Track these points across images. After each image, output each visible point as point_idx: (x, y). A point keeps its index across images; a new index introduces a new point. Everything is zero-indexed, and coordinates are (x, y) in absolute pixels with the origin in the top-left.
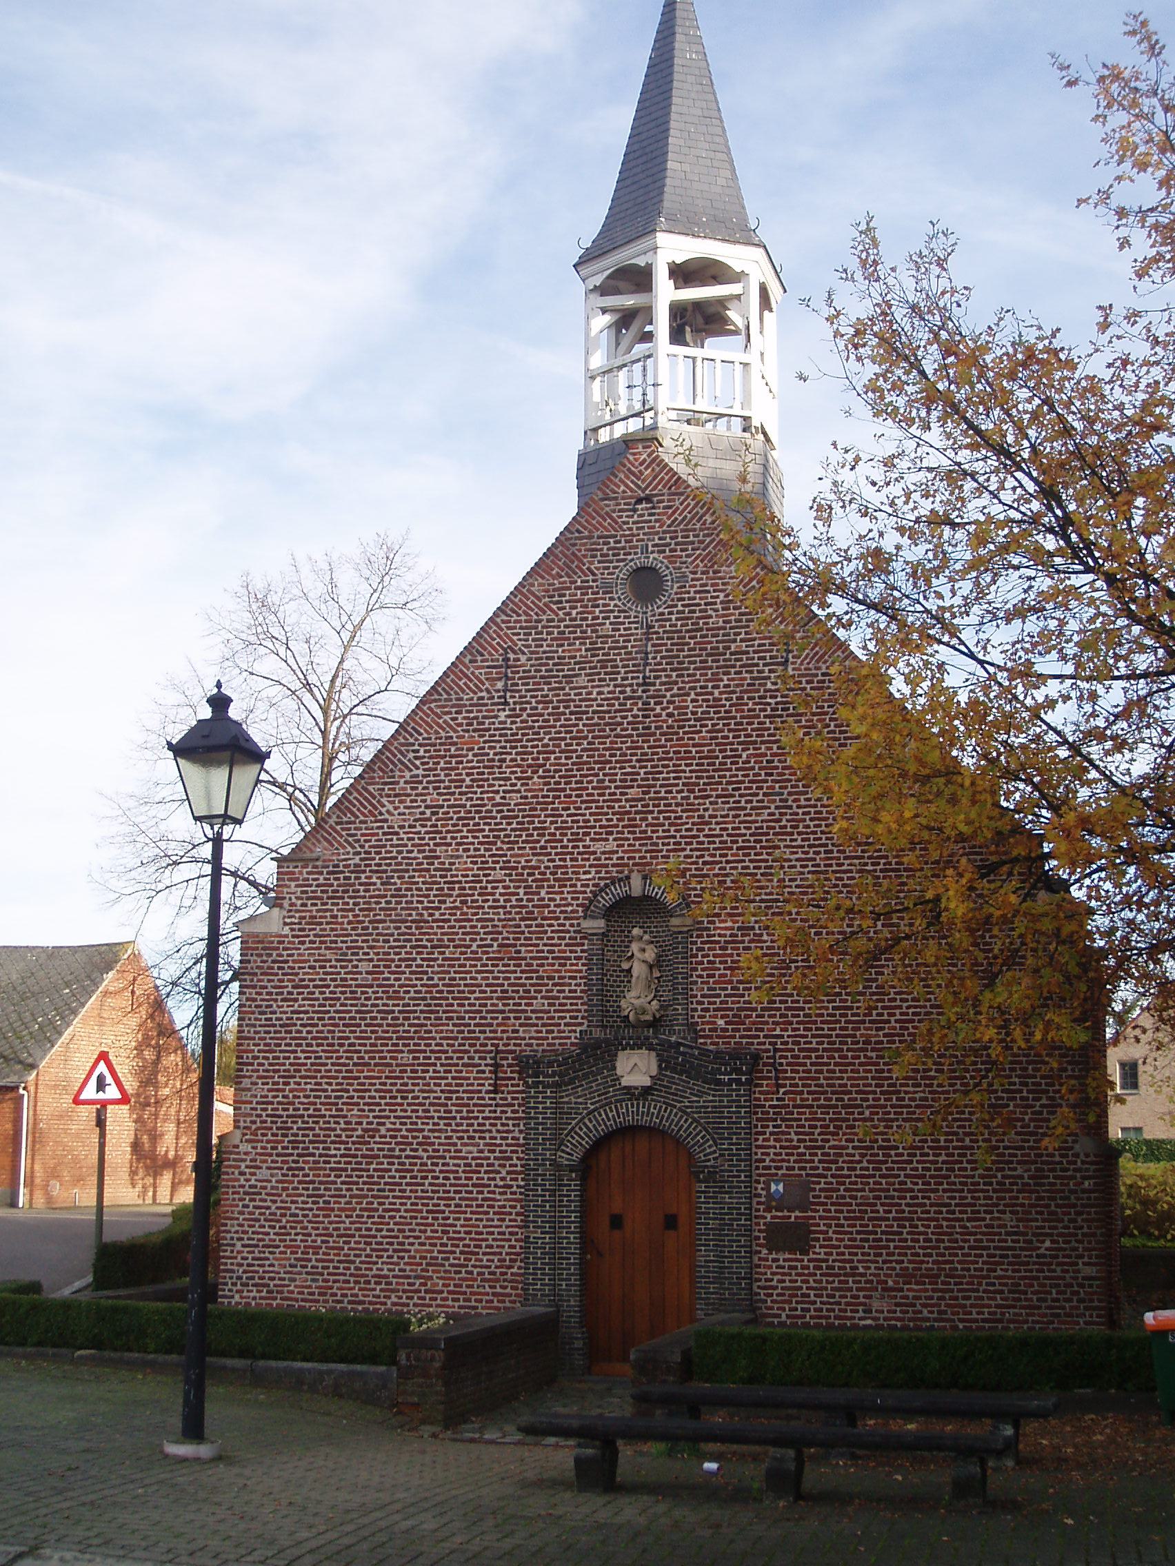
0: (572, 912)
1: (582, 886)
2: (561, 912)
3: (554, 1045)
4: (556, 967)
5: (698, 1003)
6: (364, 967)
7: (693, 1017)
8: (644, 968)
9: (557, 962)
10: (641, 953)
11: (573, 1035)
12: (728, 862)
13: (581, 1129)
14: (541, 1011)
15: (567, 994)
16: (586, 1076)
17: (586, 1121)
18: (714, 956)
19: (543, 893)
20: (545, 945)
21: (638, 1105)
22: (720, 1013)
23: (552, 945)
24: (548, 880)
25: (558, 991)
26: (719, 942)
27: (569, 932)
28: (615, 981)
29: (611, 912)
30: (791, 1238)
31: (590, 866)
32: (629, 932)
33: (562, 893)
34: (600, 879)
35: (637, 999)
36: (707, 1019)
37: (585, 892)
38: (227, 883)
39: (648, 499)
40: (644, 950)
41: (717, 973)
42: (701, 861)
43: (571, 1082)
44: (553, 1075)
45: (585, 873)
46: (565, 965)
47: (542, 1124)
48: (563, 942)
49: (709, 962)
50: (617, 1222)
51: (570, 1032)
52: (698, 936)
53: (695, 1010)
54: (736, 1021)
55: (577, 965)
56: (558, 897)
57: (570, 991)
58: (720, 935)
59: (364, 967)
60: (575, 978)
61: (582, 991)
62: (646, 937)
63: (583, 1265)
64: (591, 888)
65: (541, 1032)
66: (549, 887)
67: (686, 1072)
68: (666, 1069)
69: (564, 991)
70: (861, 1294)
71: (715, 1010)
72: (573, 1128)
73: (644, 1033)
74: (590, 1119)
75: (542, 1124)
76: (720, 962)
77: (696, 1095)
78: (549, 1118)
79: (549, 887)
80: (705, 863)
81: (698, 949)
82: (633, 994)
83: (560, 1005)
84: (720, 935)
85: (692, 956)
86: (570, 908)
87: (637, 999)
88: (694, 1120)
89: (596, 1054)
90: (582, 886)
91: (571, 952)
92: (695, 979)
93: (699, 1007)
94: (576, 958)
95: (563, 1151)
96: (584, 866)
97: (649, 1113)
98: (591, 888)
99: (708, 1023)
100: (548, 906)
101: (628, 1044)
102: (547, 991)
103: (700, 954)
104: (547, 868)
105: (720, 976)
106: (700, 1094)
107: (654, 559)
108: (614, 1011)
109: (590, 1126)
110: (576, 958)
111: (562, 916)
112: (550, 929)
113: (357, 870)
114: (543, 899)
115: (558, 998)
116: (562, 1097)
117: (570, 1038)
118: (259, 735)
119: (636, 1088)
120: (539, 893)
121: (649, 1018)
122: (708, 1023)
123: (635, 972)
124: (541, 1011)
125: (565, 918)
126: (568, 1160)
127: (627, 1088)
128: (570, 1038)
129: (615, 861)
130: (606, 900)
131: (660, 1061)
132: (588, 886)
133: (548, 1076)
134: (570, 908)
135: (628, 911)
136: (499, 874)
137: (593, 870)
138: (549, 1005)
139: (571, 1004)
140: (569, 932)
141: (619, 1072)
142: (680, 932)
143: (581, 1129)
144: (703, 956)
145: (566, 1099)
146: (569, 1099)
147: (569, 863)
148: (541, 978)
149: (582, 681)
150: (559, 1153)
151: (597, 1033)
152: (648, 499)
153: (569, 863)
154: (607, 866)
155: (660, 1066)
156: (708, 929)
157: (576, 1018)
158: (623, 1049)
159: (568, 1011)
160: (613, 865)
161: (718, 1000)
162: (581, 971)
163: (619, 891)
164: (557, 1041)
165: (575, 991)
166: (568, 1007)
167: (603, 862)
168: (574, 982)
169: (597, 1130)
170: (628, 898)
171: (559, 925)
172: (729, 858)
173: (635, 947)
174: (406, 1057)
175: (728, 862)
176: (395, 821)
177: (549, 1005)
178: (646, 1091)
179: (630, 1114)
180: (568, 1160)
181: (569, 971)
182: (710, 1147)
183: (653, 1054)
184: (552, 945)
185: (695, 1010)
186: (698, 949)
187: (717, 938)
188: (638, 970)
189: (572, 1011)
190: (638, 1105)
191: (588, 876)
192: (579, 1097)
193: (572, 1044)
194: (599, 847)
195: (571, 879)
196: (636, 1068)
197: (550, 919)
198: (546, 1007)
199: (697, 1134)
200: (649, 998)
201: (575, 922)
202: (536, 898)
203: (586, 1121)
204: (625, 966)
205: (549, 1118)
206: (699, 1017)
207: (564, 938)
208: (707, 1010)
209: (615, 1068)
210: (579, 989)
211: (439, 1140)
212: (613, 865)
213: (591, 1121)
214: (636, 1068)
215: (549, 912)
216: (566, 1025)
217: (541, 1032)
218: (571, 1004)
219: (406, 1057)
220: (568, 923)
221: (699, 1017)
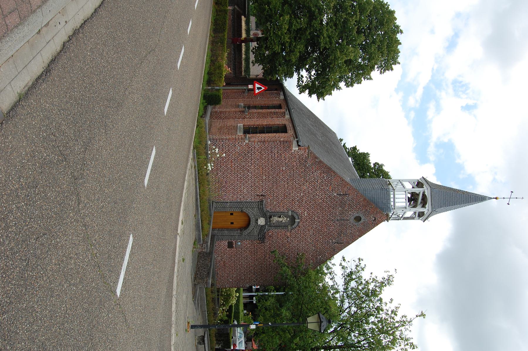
6: (284, 168)
10: (283, 220)
29: (292, 216)
30: (230, 245)
38: (19, 71)
39: (375, 220)
50: (232, 223)
54: (270, 236)
59: (284, 168)
63: (274, 132)
74: (252, 213)
89: (264, 215)
97: (253, 223)
107: (362, 221)
113: (305, 166)
130: (295, 215)
136: (302, 195)
149: (340, 209)
152: (375, 220)
163: (296, 217)
170: (295, 219)
173: (285, 219)
174: (264, 178)
176: (315, 174)
188: (281, 219)
194: (306, 213)
196: (262, 221)
211: (247, 185)
219: (264, 178)
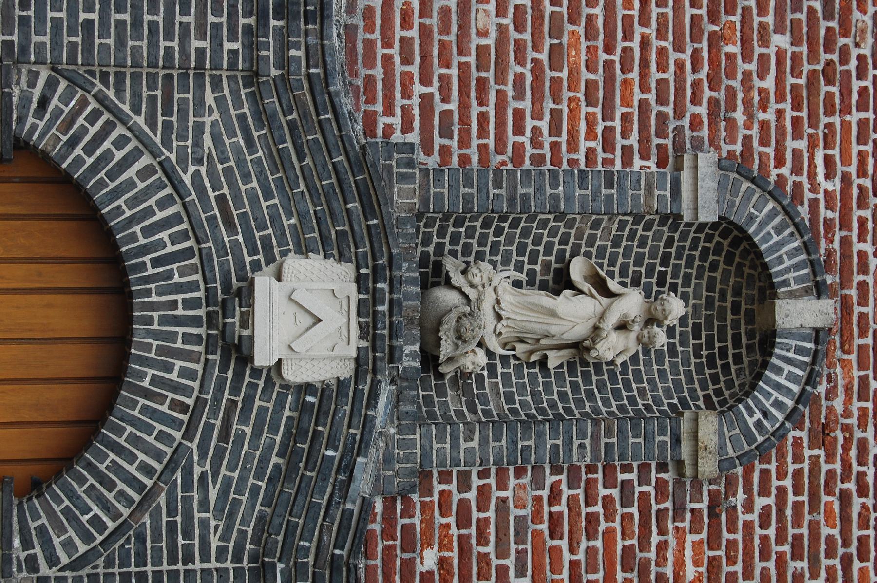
0: (731, 124)
1: (797, 154)
2: (731, 93)
3: (369, 62)
4: (586, 75)
5: (483, 493)
7: (445, 477)
8: (578, 331)
9: (598, 77)
11: (396, 121)
12: (847, 562)
13: (120, 143)
14: (463, 28)
15: (512, 105)
16: (280, 161)
17: (145, 160)
18: (609, 534)
19: (780, 41)
20: (645, 43)
21: (195, 321)
22: (454, 555)
23: (645, 63)
24: (813, 56)
25: (519, 79)
26: (644, 545)
27: (679, 113)
28: (537, 241)
29: (731, 242)
31: (846, 179)
32: (674, 288)
33: (780, 98)
34: (814, 203)
35: (499, 306)
36: (439, 520)
37: (780, 162)
40: (622, 327)
41: (564, 544)
42: (851, 486)
43: (263, 116)
44: (284, 62)
45: (829, 161)
46: (590, 101)
47: (137, 23)
48: (652, 97)
49: (592, 519)
51: (406, 112)
52: (661, 486)
53: (464, 484)
55: (591, 134)
56: (769, 84)
57: (519, 115)
58: (662, 547)
60: (555, 129)
61: (518, 149)
62: (661, 339)
64: (791, 179)
65: (406, 23)
66: (796, 57)
67: (292, 467)
68: (303, 408)
69: (519, 95)
70: (771, 565)
71: (463, 541)
72: (120, 117)
73: (402, 331)
75: (137, 23)
76: (591, 552)
77: (224, 493)
78: (153, 44)
79: (796, 57)
80: (845, 498)
81: (626, 486)
82: (510, 298)
83: (482, 84)
84: (662, 547)
85: (609, 471)
86: (739, 116)
87: (499, 306)
88: (149, 496)
89: (350, 203)
90: (797, 154)
91: (626, 118)
92: (550, 479)
93: (472, 495)
94: (608, 131)
95: (51, 85)
96: (846, 161)
97: (168, 355)
98: (791, 179)
99: (428, 523)
100: (747, 56)
101: (376, 299)
102: (519, 46)
103: (615, 492)
104: (844, 58)
105: (555, 552)
106: (227, 511)
108: (455, 239)
109: (131, 173)
110: (608, 131)
111: (721, 95)
112: (686, 57)
114: (764, 41)
115: (500, 78)
116: (216, 85)
117: (389, 111)
118: (860, 505)
119: (247, 321)
120: (779, 29)
121: (446, 349)
122: (428, 523)
123: (565, 302)
124: (463, 28)
125: (713, 104)
126: (25, 100)
127: (246, 294)
128: (389, 111)
129: (857, 247)
131: (323, 391)
132: (797, 170)
133: (283, 47)
134: (739, 116)
135: (731, 278)
137: (835, 186)
138: (482, 51)
139: (483, 118)
140: (679, 113)
141: (293, 264)
142: (677, 440)
143: (120, 143)
144: (608, 501)
145: (210, 98)
146: (216, 109)
147: (855, 117)
148: (556, 31)
150: (44, 74)
151: (402, 198)
153: (855, 117)
154: (845, 224)
155: (307, 388)
156: (679, 512)
157: (446, 133)
158: (359, 280)
159: (464, 107)
160: (846, 243)
161: (490, 549)
162: (573, 146)
163: (784, 258)
164: (378, 72)
165: (519, 130)
166: (475, 109)
167: (857, 213)
168: (544, 125)
169: (116, 193)
170: (768, 291)
171: (696, 84)
172: (857, 565)
173: (632, 303)
175: (847, 562)
177: (482, 51)
178: (238, 352)
179: (168, 307)
180: (25, 100)
181: (573, 113)
182: (68, 545)
183: (346, 371)
184: (645, 63)
185: (464, 484)
186: (626, 486)
187: (655, 539)
188: (574, 313)
189: (464, 120)
190: (195, 321)
191: (821, 170)
192: (217, 139)
193: (370, 120)
195: (814, 123)
197: (714, 62)
198: (475, 41)
199: (106, 506)
200: (494, 345)
201: (705, 132)
202: (770, 19)
203: (145, 160)
204: (577, 270)
205: (153, 44)
206: (445, 496)
207: (662, 100)
208: (463, 520)
209: (304, 249)
210: (525, 139)
212: (846, 243)
213: (144, 174)
214: (306, 318)
215: (730, 57)
216: (426, 99)
217: (406, 23)
218: (483, 118)
220: (702, 110)
221: (445, 496)
